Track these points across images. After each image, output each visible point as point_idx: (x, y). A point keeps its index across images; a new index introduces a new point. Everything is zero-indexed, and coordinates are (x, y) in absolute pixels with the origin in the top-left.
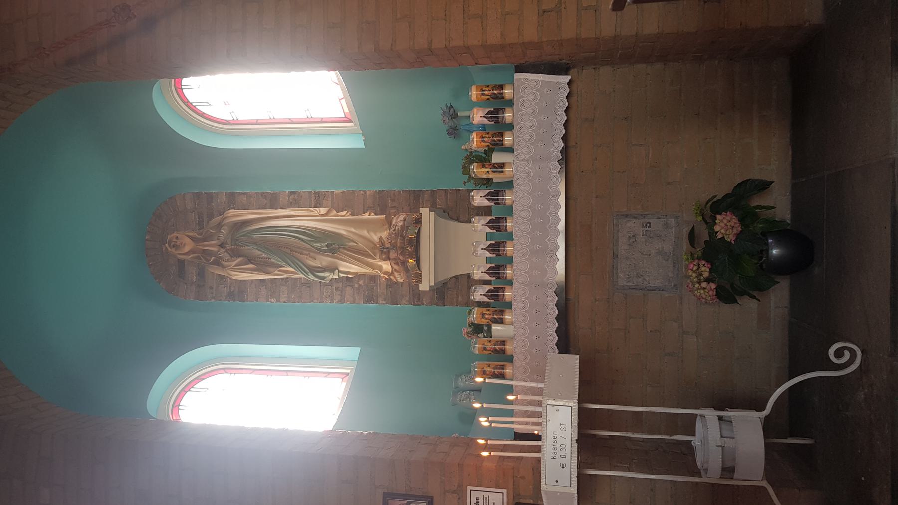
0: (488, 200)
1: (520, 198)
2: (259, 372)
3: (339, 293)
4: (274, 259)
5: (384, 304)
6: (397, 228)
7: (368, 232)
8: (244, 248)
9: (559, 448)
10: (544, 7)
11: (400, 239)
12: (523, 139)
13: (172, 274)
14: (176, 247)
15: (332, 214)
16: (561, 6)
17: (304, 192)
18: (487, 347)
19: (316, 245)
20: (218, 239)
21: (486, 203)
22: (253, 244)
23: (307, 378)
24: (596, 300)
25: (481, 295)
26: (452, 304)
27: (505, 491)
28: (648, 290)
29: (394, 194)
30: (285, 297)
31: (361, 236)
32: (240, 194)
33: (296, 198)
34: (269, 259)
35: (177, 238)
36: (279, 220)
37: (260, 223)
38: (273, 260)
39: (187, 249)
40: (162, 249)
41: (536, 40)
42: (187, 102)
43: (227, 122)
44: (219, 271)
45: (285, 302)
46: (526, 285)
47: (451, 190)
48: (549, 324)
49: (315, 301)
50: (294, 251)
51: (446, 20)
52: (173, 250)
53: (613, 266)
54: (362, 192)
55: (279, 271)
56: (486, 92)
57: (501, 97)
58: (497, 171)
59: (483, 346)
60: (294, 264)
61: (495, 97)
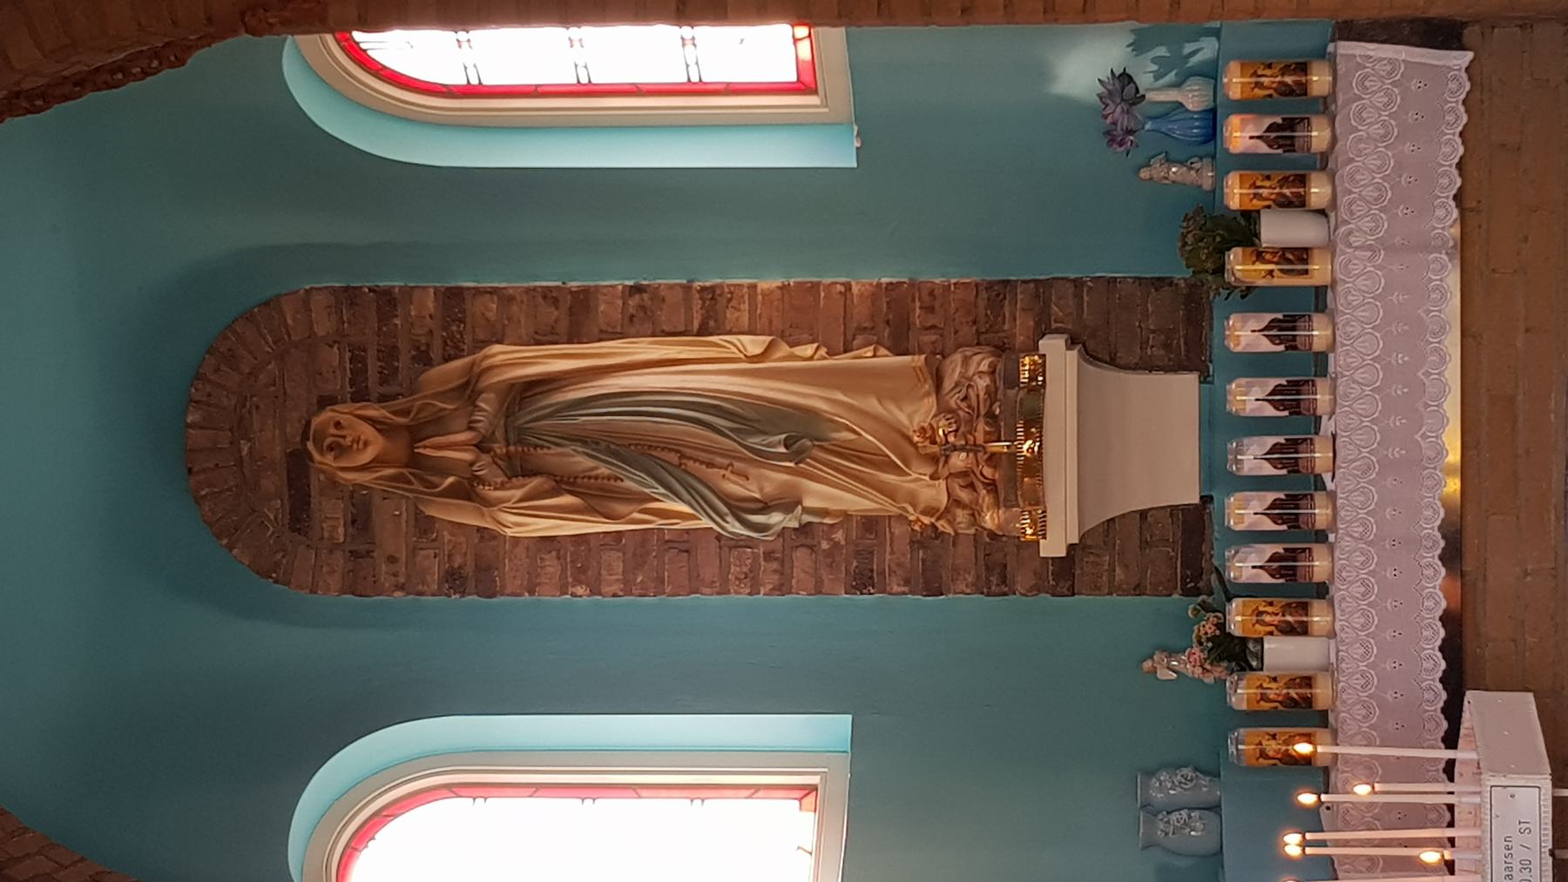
0: (1271, 338)
3: (775, 565)
5: (904, 593)
6: (972, 394)
9: (1517, 866)
12: (1362, 198)
13: (270, 521)
15: (778, 354)
17: (671, 287)
18: (1268, 691)
20: (470, 428)
23: (699, 801)
24: (1526, 574)
26: (1096, 589)
29: (931, 293)
30: (617, 580)
31: (867, 414)
32: (478, 292)
33: (648, 303)
34: (617, 479)
35: (338, 425)
36: (617, 376)
39: (367, 456)
45: (615, 595)
46: (1370, 543)
47: (1094, 279)
48: (1425, 633)
49: (704, 590)
50: (690, 458)
52: (329, 458)
54: (838, 286)
55: (641, 511)
57: (1302, 89)
58: (1292, 270)
59: (1260, 691)
61: (1286, 91)
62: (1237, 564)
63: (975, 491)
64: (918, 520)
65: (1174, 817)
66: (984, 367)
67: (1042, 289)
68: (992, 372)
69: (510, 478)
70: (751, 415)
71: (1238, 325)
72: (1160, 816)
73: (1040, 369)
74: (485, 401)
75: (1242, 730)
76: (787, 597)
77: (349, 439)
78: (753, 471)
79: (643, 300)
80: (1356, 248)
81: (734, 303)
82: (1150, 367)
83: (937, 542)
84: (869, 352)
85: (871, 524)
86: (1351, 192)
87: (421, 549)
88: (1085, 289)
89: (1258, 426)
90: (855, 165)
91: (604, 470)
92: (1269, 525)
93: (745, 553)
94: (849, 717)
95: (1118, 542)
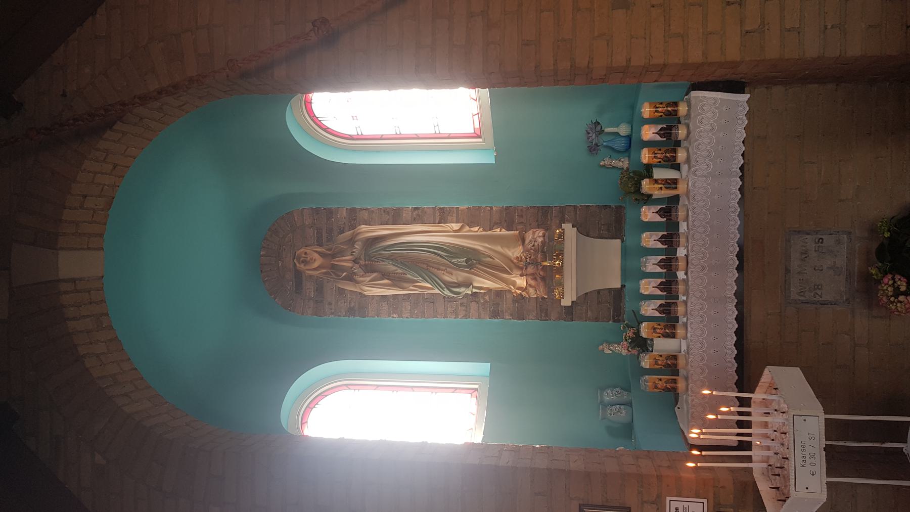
1: (699, 214)
2: (365, 387)
4: (410, 275)
5: (510, 319)
6: (536, 244)
7: (502, 247)
8: (379, 263)
9: (808, 456)
10: (747, 28)
11: (541, 255)
13: (288, 289)
14: (305, 262)
15: (465, 230)
16: (764, 27)
18: (658, 361)
19: (454, 260)
20: (351, 255)
21: (658, 219)
22: (388, 259)
25: (652, 309)
26: (580, 319)
27: (705, 501)
28: (821, 304)
29: (522, 210)
33: (420, 213)
34: (404, 274)
35: (306, 253)
37: (396, 238)
38: (409, 276)
39: (316, 265)
40: (279, 265)
41: (738, 60)
42: (313, 117)
43: (351, 138)
44: (349, 287)
45: (407, 318)
47: (581, 206)
50: (431, 267)
51: (645, 39)
52: (302, 265)
53: (786, 280)
55: (413, 286)
56: (660, 109)
58: (670, 187)
60: (431, 280)
61: (668, 114)
62: (645, 308)
63: (537, 281)
64: (516, 291)
65: (614, 408)
66: (541, 234)
67: (562, 210)
68: (544, 236)
69: (366, 273)
70: (454, 251)
71: (647, 211)
72: (608, 407)
73: (562, 235)
74: (357, 245)
75: (647, 376)
76: (468, 319)
77: (309, 258)
78: (454, 272)
79: (418, 212)
80: (699, 176)
81: (451, 214)
82: (601, 237)
83: (523, 300)
84: (498, 230)
85: (499, 293)
86: (697, 153)
87: (60, 236)
88: (578, 209)
89: (653, 252)
90: (494, 163)
91: (400, 271)
92: (659, 292)
93: (453, 303)
94: (489, 364)
95: (589, 302)
